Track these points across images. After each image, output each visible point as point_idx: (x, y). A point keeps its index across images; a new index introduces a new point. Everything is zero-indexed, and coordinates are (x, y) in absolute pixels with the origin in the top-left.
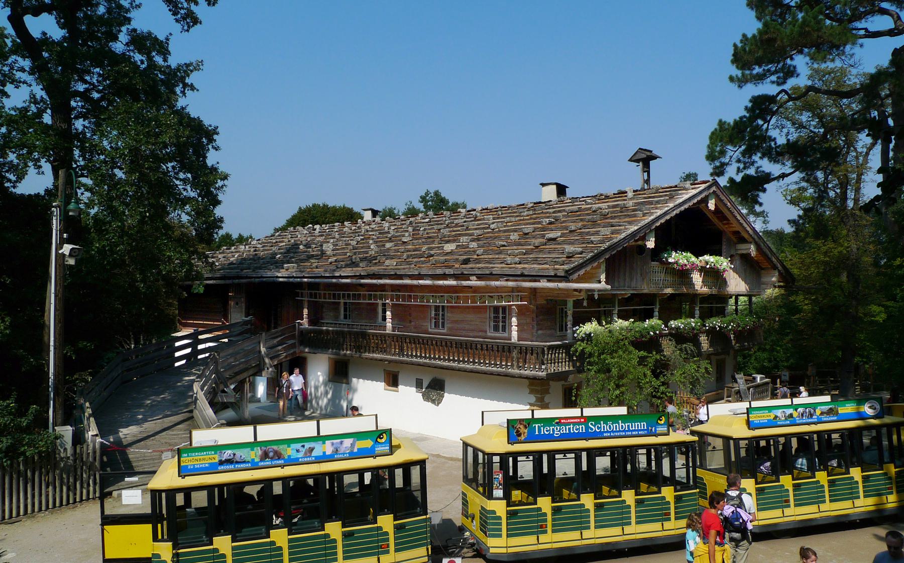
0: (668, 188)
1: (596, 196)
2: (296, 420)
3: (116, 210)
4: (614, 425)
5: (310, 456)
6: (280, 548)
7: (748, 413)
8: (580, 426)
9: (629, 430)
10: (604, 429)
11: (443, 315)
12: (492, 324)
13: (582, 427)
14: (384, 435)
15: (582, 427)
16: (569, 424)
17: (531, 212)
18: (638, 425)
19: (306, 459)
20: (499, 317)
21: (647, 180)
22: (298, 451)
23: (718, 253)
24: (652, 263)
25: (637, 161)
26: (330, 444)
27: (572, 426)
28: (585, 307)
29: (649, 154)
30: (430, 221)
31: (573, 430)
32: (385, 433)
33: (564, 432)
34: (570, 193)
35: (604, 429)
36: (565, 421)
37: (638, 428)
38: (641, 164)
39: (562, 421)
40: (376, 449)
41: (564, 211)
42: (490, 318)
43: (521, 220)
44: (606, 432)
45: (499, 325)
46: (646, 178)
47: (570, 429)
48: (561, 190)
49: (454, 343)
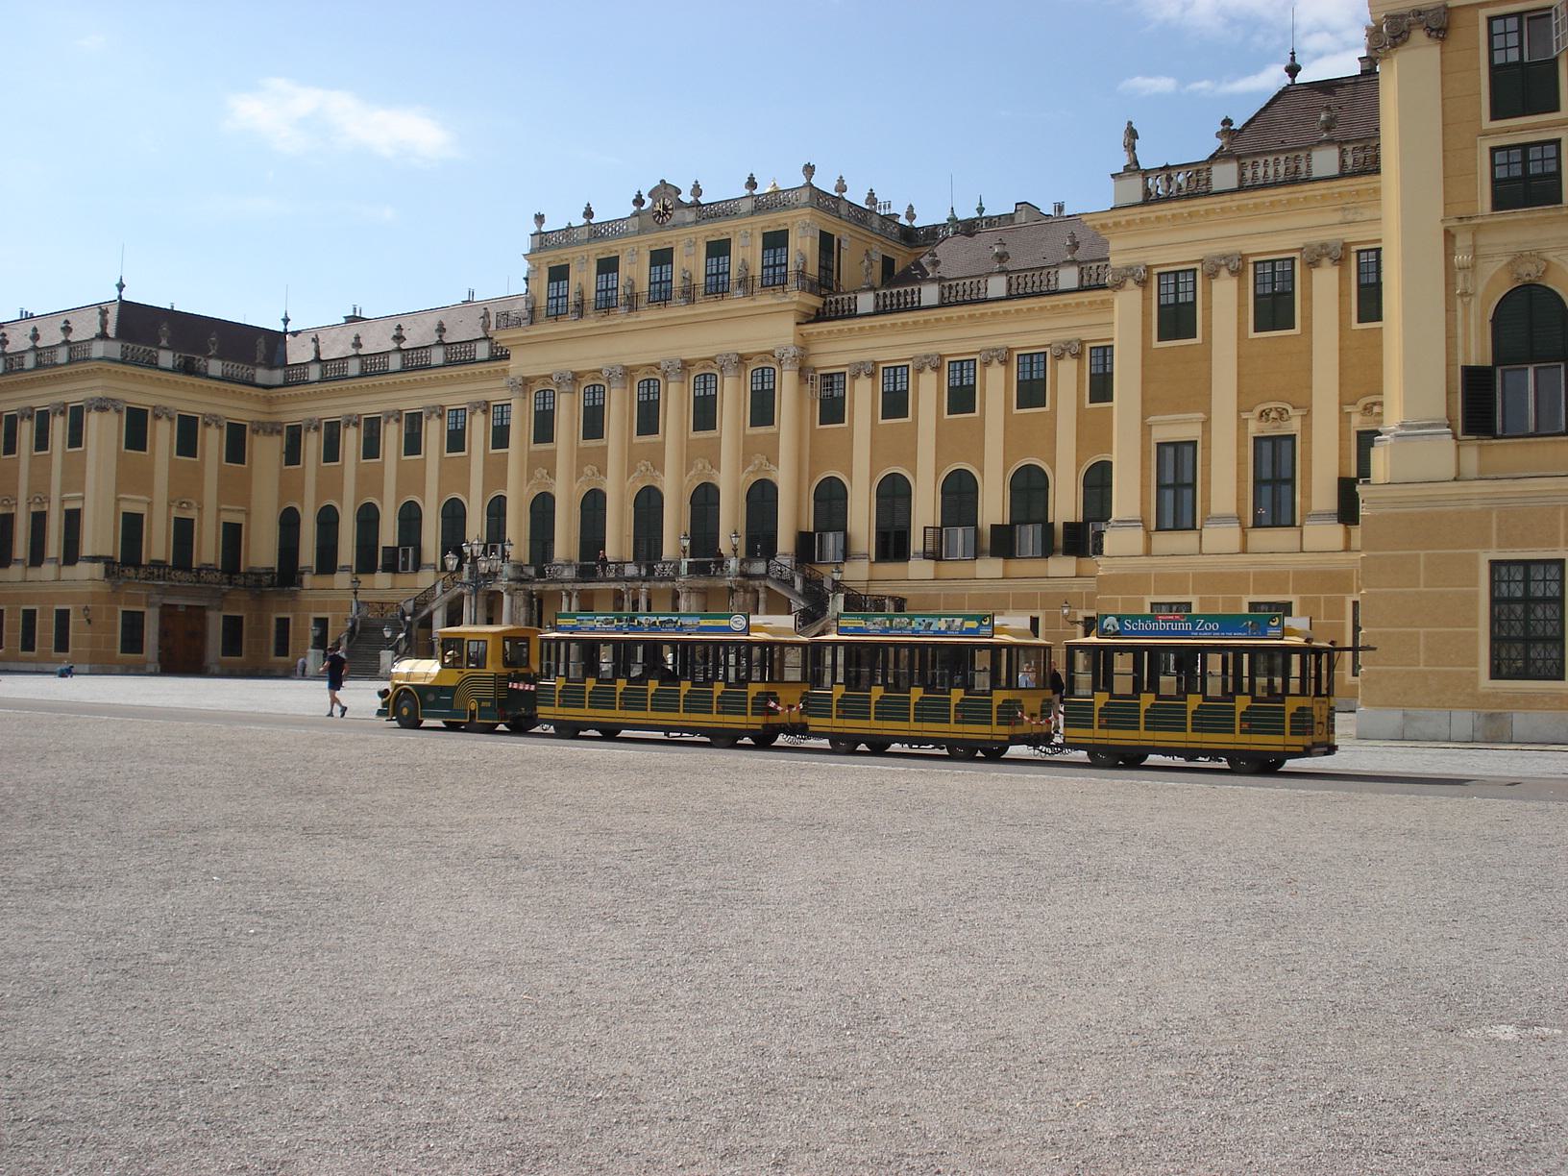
2: (91, 673)
22: (920, 624)
23: (287, 612)
49: (864, 652)
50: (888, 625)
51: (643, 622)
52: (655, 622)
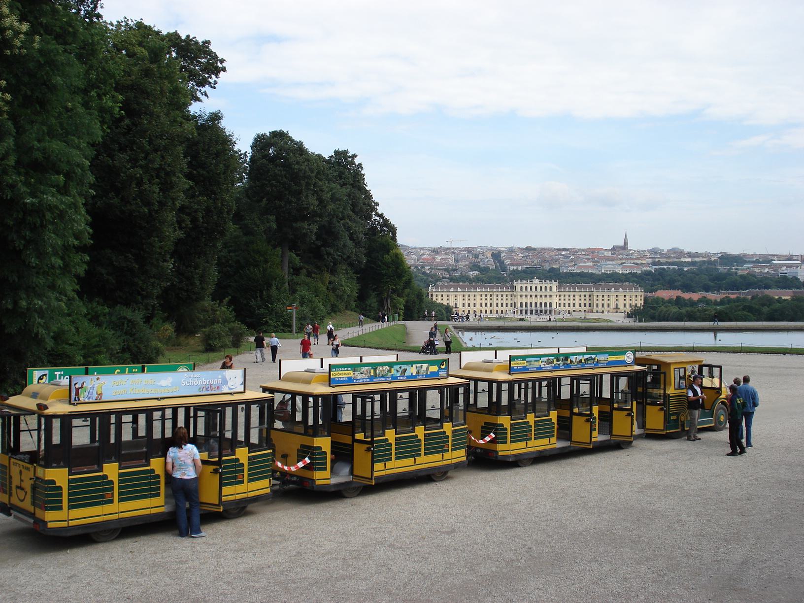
3: (317, 172)
5: (404, 376)
6: (60, 488)
19: (401, 378)
22: (397, 371)
26: (415, 367)
40: (440, 373)
50: (372, 374)
51: (574, 360)
52: (581, 360)
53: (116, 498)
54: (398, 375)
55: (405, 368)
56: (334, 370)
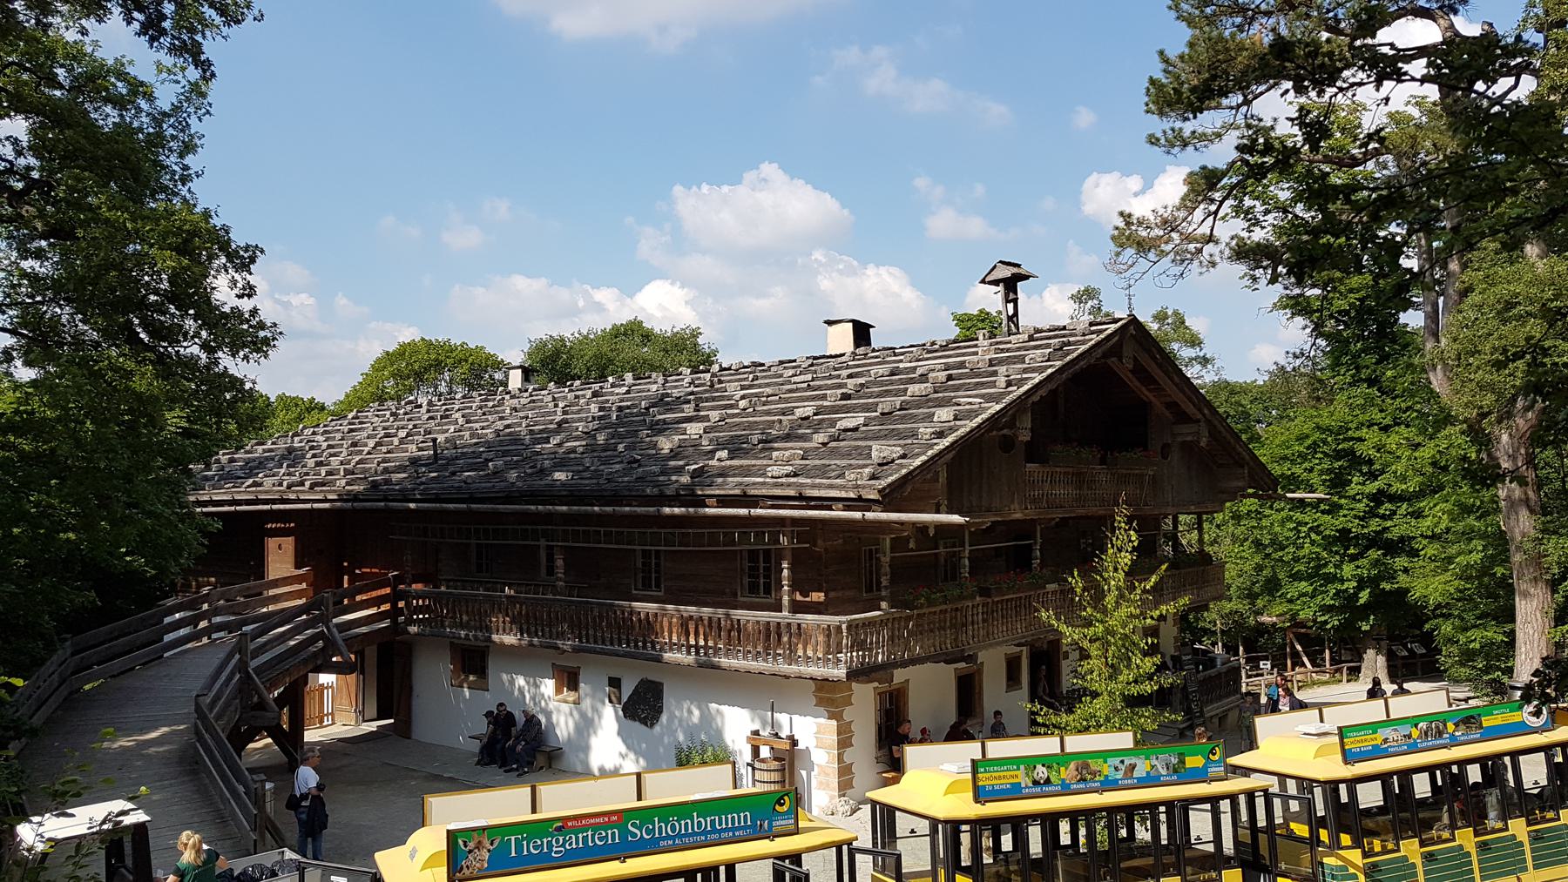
0: (1050, 331)
1: (924, 345)
4: (683, 822)
5: (1132, 777)
7: (975, 771)
8: (609, 832)
9: (714, 831)
10: (660, 833)
11: (658, 565)
12: (746, 580)
13: (613, 833)
14: (786, 798)
15: (613, 833)
16: (585, 828)
17: (809, 377)
18: (733, 818)
20: (758, 567)
21: (1013, 315)
22: (1116, 769)
24: (1028, 465)
25: (996, 283)
27: (590, 833)
28: (912, 550)
29: (1015, 270)
30: (628, 392)
31: (593, 841)
32: (787, 795)
33: (574, 846)
34: (877, 340)
35: (660, 833)
36: (575, 823)
37: (733, 823)
38: (1001, 288)
39: (570, 824)
41: (1048, 346)
42: (742, 570)
43: (791, 391)
44: (664, 839)
45: (759, 583)
46: (1011, 312)
47: (585, 839)
48: (862, 332)
53: (1530, 863)
54: (1119, 777)
55: (1132, 762)
56: (982, 770)
